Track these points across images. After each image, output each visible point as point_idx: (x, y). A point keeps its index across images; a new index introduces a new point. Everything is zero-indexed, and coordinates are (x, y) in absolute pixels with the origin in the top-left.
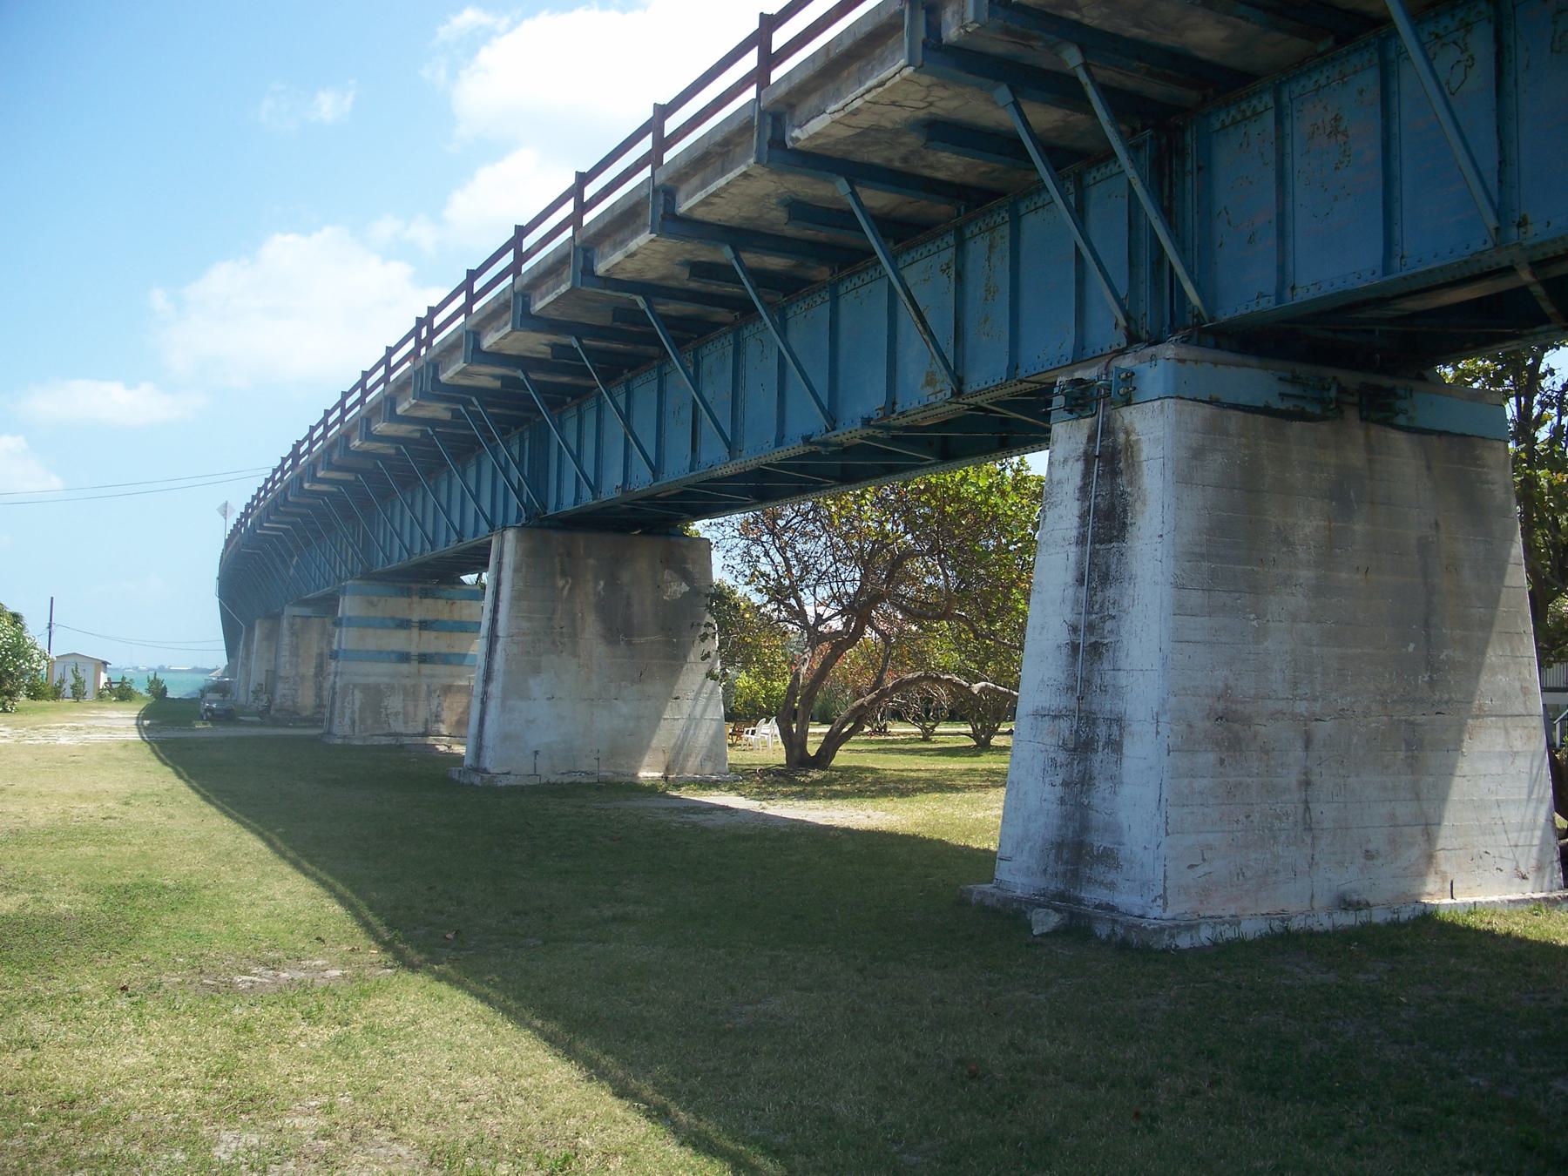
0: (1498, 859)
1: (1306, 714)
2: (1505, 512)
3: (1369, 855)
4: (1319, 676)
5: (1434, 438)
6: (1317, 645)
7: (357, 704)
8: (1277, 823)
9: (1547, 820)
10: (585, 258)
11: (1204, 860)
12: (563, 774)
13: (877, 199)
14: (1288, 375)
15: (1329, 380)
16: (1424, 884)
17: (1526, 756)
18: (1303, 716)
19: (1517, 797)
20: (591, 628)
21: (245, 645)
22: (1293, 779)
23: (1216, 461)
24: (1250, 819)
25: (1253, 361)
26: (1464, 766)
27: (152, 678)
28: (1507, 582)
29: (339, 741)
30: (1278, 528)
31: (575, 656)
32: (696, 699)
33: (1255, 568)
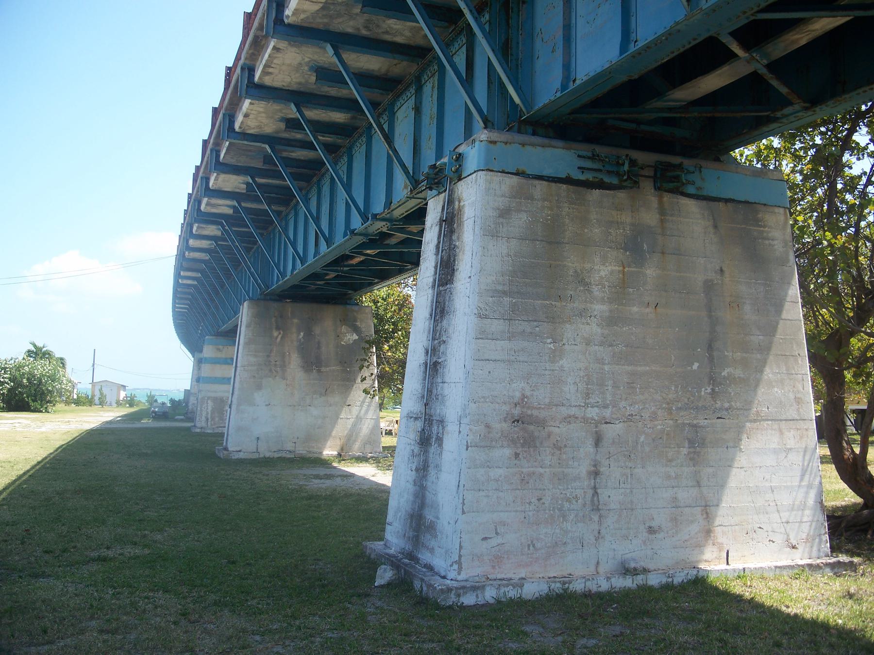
0: (770, 533)
1: (596, 418)
2: (784, 262)
3: (651, 530)
4: (610, 388)
5: (721, 204)
6: (609, 364)
7: (210, 408)
8: (567, 505)
9: (816, 502)
10: (230, 120)
11: (497, 533)
12: (275, 452)
14: (590, 154)
15: (624, 157)
16: (702, 553)
17: (798, 452)
18: (595, 420)
19: (789, 484)
20: (295, 361)
22: (583, 468)
23: (520, 220)
24: (541, 501)
25: (560, 143)
26: (741, 460)
27: (149, 394)
28: (784, 315)
29: (198, 430)
30: (576, 272)
31: (284, 379)
32: (361, 406)
33: (553, 303)
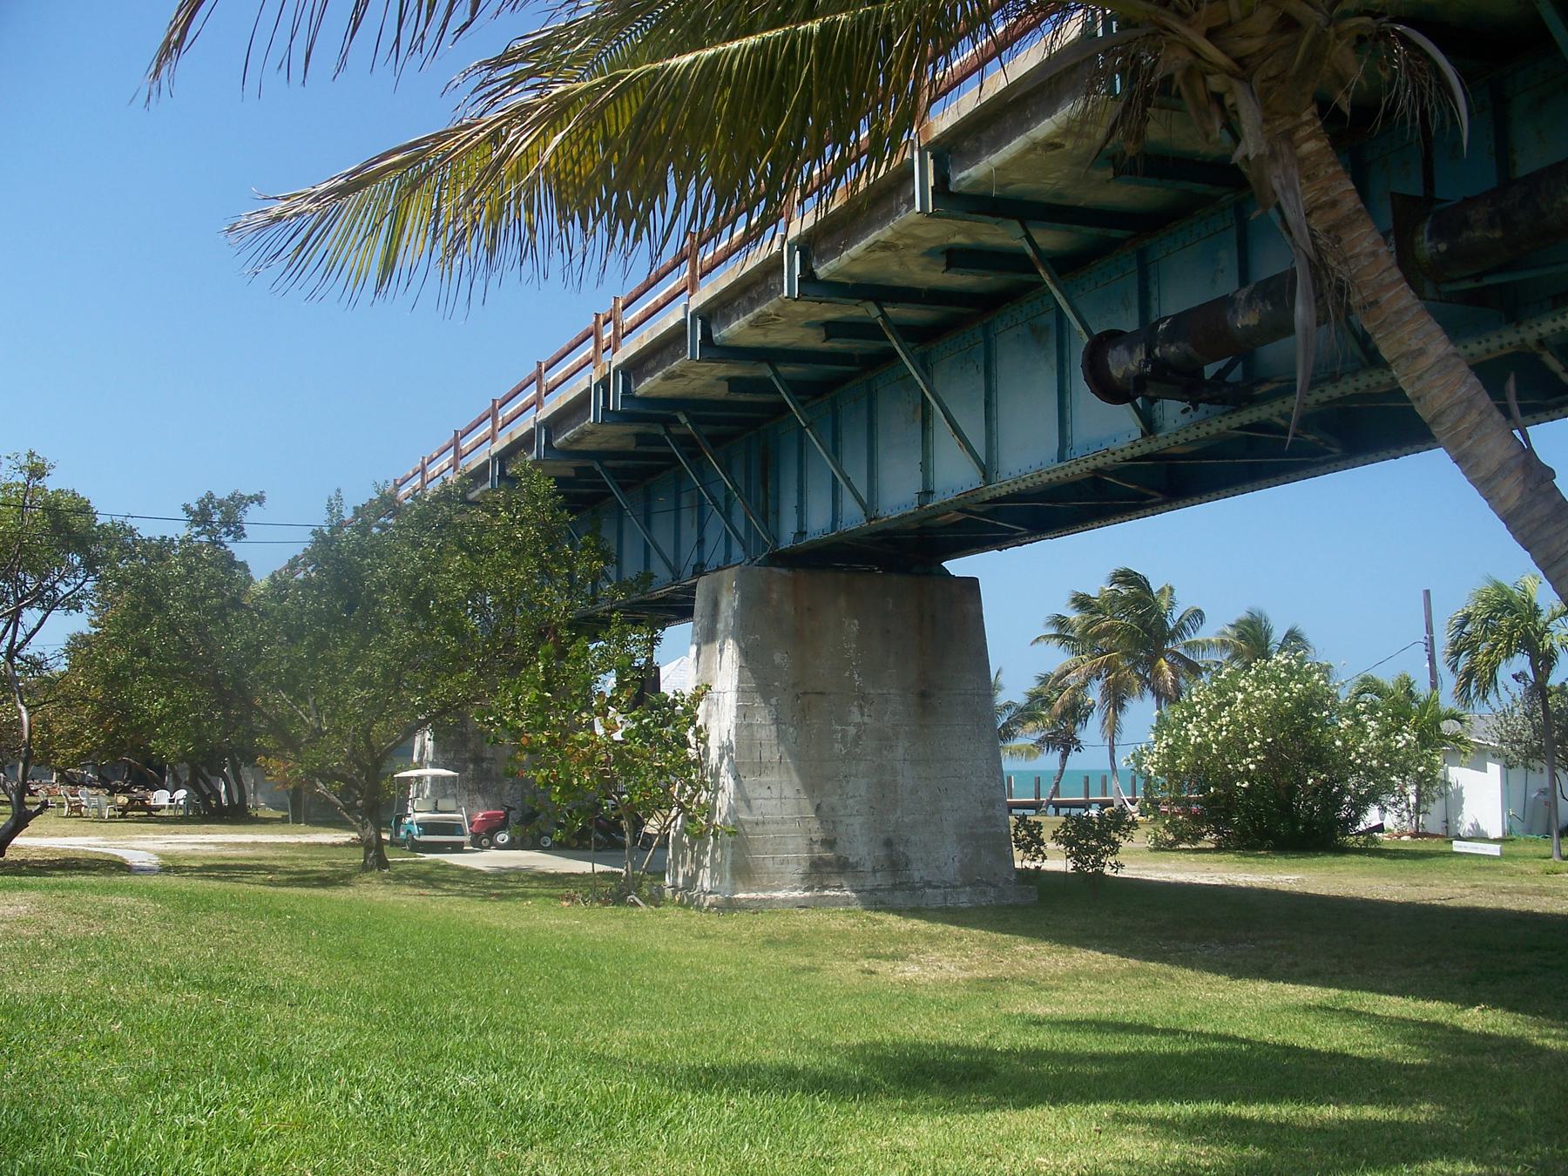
13: (1049, 238)
21: (1215, 1120)
